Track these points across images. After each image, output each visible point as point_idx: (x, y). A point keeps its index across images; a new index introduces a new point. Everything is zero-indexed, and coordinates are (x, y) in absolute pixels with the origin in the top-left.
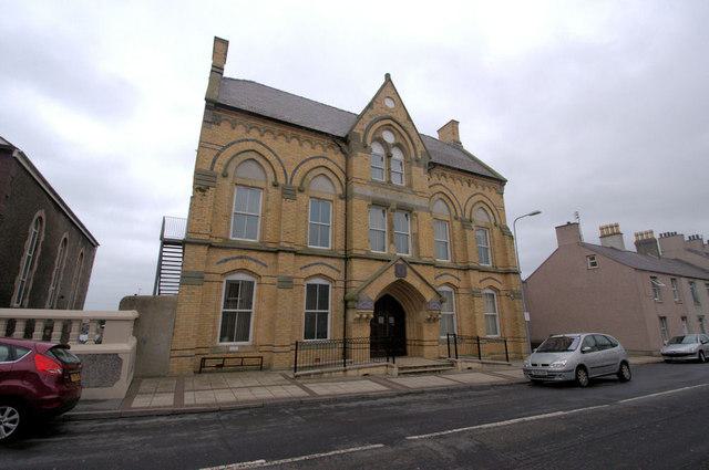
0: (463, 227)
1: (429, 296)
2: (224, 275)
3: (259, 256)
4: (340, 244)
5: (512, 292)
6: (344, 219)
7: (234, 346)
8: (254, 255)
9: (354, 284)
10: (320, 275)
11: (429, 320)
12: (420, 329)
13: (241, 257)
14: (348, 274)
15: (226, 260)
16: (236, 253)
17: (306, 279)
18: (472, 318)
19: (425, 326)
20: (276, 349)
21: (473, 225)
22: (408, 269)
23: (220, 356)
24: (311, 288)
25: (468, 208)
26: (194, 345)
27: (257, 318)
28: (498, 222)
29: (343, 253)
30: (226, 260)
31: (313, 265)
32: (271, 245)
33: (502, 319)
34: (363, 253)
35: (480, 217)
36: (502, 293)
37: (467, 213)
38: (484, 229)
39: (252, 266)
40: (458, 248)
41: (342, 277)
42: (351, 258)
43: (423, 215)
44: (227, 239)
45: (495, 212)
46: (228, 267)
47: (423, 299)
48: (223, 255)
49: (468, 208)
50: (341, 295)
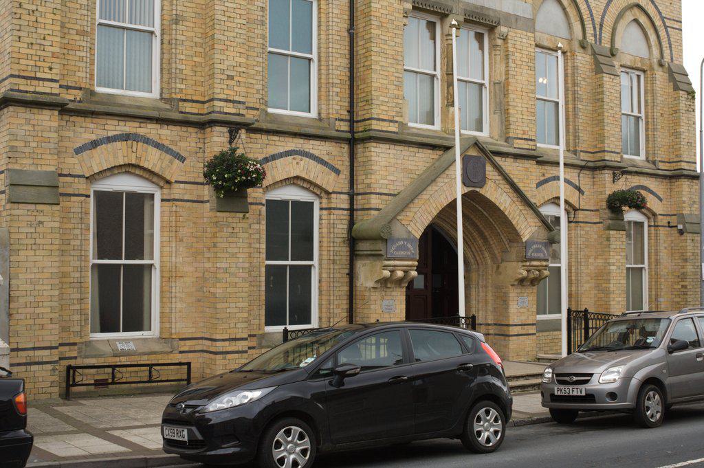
0: (598, 69)
1: (527, 228)
2: (92, 178)
3: (166, 134)
4: (338, 107)
5: (681, 217)
6: (346, 43)
7: (123, 339)
8: (150, 130)
9: (375, 201)
10: (295, 181)
11: (522, 281)
12: (503, 301)
13: (126, 137)
14: (360, 178)
15: (94, 144)
16: (114, 127)
17: (92, 178)
18: (602, 276)
19: (513, 294)
20: (220, 346)
21: (616, 63)
22: (489, 168)
23: (101, 362)
24: (107, 203)
25: (609, 20)
26: (54, 340)
27: (167, 278)
28: (667, 58)
29: (344, 126)
30: (94, 144)
31: (281, 155)
32: (189, 108)
33: (655, 278)
34: (393, 128)
35: (631, 44)
36: (662, 221)
37: (606, 35)
38: (640, 69)
39: (152, 159)
40: (582, 119)
41: (342, 183)
42: (364, 140)
43: (520, 40)
44: (93, 93)
45: (662, 33)
46: (99, 159)
47: (514, 235)
48: (87, 130)
49: (609, 20)
50: (342, 227)
